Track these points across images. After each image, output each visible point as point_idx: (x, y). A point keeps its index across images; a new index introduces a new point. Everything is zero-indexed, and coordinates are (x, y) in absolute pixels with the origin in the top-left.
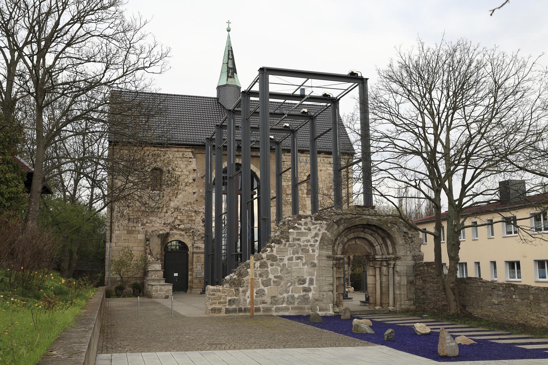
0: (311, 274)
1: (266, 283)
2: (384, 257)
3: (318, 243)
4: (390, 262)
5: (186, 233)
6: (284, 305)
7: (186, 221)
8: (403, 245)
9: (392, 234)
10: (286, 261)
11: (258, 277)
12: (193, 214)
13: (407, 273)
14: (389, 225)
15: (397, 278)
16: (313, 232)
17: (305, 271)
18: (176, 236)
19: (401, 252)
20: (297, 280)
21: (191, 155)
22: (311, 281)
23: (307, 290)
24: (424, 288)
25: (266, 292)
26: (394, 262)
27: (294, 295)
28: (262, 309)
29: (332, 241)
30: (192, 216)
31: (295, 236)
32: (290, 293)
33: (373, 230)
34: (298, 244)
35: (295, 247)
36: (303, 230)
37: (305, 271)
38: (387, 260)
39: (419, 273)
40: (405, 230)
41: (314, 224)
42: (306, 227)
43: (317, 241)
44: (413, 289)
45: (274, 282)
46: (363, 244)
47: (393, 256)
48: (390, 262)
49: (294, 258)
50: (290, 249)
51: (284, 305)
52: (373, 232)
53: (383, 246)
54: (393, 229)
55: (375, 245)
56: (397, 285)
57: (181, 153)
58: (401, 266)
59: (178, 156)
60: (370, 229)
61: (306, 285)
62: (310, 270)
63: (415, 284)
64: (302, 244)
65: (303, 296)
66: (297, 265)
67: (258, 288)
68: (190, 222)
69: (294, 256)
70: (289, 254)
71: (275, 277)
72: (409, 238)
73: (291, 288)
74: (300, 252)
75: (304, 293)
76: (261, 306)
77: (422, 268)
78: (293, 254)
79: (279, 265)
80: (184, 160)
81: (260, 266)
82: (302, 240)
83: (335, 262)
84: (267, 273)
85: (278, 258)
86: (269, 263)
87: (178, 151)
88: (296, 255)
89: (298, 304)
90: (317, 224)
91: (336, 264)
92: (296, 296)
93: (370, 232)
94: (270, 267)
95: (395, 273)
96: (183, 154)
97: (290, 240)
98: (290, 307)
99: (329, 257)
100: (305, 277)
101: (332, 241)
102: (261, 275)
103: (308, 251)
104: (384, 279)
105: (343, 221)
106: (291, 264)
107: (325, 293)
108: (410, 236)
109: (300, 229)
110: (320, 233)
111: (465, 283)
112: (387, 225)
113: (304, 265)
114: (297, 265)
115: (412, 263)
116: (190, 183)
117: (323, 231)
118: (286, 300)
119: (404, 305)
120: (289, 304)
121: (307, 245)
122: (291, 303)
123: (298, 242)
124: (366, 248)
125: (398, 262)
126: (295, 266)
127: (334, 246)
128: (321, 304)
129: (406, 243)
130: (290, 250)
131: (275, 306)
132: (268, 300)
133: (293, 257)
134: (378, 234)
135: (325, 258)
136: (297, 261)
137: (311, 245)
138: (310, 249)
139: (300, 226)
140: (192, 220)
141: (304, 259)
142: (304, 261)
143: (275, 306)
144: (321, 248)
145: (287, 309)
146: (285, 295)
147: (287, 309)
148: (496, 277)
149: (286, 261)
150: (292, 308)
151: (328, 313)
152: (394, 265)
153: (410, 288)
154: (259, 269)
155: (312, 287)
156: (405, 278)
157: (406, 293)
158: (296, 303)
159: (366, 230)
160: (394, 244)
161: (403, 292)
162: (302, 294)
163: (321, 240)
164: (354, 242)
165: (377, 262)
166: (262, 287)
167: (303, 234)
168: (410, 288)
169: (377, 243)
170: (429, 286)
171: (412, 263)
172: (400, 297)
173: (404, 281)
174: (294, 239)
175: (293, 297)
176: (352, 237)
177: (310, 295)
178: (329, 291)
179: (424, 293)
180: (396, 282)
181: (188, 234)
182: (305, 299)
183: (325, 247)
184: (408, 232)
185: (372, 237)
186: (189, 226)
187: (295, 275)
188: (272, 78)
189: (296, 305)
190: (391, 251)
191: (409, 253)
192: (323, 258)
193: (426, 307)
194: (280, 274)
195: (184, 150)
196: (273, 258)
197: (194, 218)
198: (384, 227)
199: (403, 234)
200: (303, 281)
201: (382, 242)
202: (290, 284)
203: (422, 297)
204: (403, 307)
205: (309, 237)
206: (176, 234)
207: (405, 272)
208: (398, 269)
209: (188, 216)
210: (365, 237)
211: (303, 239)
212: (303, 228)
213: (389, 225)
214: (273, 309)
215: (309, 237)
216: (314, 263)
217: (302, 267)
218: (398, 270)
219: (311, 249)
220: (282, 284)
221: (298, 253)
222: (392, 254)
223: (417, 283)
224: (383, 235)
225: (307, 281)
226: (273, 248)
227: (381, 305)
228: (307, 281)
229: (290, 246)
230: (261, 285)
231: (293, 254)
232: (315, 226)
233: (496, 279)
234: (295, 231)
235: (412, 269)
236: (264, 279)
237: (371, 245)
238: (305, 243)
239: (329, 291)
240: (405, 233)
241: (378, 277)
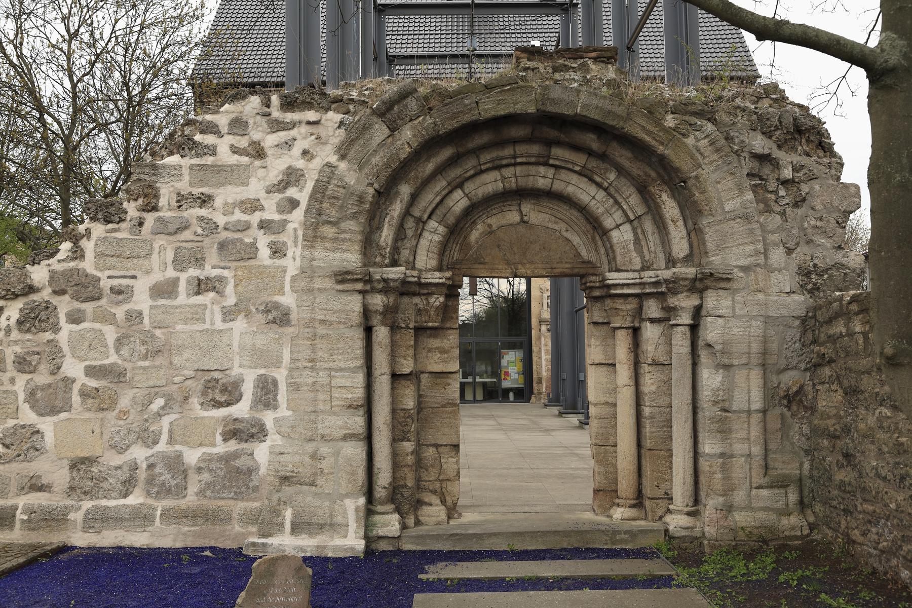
0: (260, 357)
1: (50, 401)
2: (649, 276)
3: (298, 215)
4: (673, 301)
6: (135, 499)
8: (747, 218)
9: (678, 160)
10: (142, 301)
11: (11, 371)
13: (764, 353)
14: (670, 121)
15: (710, 379)
16: (276, 166)
17: (238, 345)
19: (730, 251)
20: (196, 386)
22: (267, 393)
23: (245, 432)
24: (847, 430)
25: (49, 438)
26: (694, 301)
27: (179, 456)
28: (20, 516)
29: (361, 199)
31: (184, 185)
32: (162, 446)
33: (590, 153)
34: (201, 219)
35: (187, 235)
36: (225, 156)
37: (238, 345)
38: (663, 292)
39: (827, 350)
40: (760, 144)
41: (277, 126)
42: (243, 142)
43: (294, 204)
44: (799, 430)
45: (85, 394)
46: (562, 226)
47: (690, 271)
48: (673, 301)
49: (182, 287)
50: (160, 241)
51: (135, 499)
52: (593, 163)
53: (648, 225)
54: (690, 141)
55: (608, 223)
56: (708, 411)
58: (731, 320)
60: (576, 148)
61: (242, 409)
62: (261, 341)
63: (812, 409)
64: (221, 220)
65: (227, 459)
66: (197, 315)
67: (11, 423)
69: (183, 277)
70: (160, 265)
71: (91, 371)
72: (785, 183)
73: (166, 421)
74: (212, 256)
75: (233, 446)
76: (22, 501)
77: (839, 328)
78: (179, 263)
79: (108, 318)
81: (20, 323)
82: (218, 202)
84: (55, 353)
85: (106, 284)
86: (64, 305)
88: (193, 272)
89: (201, 493)
90: (293, 125)
92: (192, 457)
93: (580, 159)
94: (66, 329)
95: (703, 354)
97: (163, 202)
98: (160, 505)
99: (342, 277)
100: (236, 371)
101: (361, 199)
102: (23, 364)
103: (251, 251)
105: (412, 104)
106: (166, 310)
107: (324, 449)
108: (787, 173)
109: (212, 150)
110: (312, 170)
112: (658, 123)
113: (229, 315)
114: (197, 315)
115: (799, 302)
117: (327, 155)
118: (142, 475)
119: (749, 508)
120: (158, 496)
121: (247, 227)
122: (165, 491)
123: (203, 212)
124: (576, 240)
125: (712, 300)
126: (186, 321)
128: (307, 499)
129: (768, 210)
130: (164, 250)
131: (87, 504)
132: (60, 476)
133: (175, 282)
134: (621, 171)
135: (329, 283)
136: (199, 299)
137: (264, 225)
138: (263, 242)
139: (209, 139)
141: (230, 289)
142: (231, 300)
143: (87, 504)
144: (312, 237)
145: (141, 517)
146: (139, 454)
147: (141, 517)
149: (142, 301)
150: (167, 516)
151: (338, 542)
152: (697, 312)
153: (785, 428)
154: (15, 335)
155: (268, 418)
156: (756, 377)
157: (757, 450)
158: (193, 488)
159: (558, 152)
160: (692, 211)
161: (739, 448)
162: (221, 448)
163: (312, 197)
164: (513, 216)
165: (619, 304)
166: (28, 416)
167: (224, 174)
168: (785, 428)
169: (618, 216)
170: (872, 420)
171: (799, 302)
172: (725, 468)
173: (749, 391)
174: (182, 200)
175: (175, 464)
176: (490, 189)
177: (262, 453)
178: (346, 438)
179: (847, 456)
180: (705, 394)
182: (235, 476)
183: (329, 231)
184: (777, 154)
185: (593, 190)
187: (186, 362)
189: (191, 499)
190: (680, 246)
191: (777, 256)
192: (318, 283)
193: (856, 535)
194: (113, 358)
196: (83, 288)
198: (638, 128)
199: (748, 165)
200: (225, 390)
201: (640, 210)
202: (160, 402)
203: (840, 476)
204: (741, 518)
205: (255, 189)
207: (756, 347)
208: (712, 331)
210: (558, 186)
211: (224, 195)
212: (223, 145)
213: (670, 121)
214: (77, 517)
215: (255, 189)
216: (277, 306)
217: (219, 325)
219: (263, 242)
220: (124, 402)
221: (199, 261)
222: (688, 259)
223: (822, 403)
224: (636, 169)
225: (248, 390)
226: (84, 243)
227: (639, 500)
228: (248, 390)
229: (163, 229)
230: (25, 408)
231: (179, 263)
232: (283, 135)
234: (187, 162)
235: (794, 333)
236: (42, 378)
237: (596, 228)
238: (238, 216)
239: (346, 438)
240: (763, 158)
241: (624, 374)
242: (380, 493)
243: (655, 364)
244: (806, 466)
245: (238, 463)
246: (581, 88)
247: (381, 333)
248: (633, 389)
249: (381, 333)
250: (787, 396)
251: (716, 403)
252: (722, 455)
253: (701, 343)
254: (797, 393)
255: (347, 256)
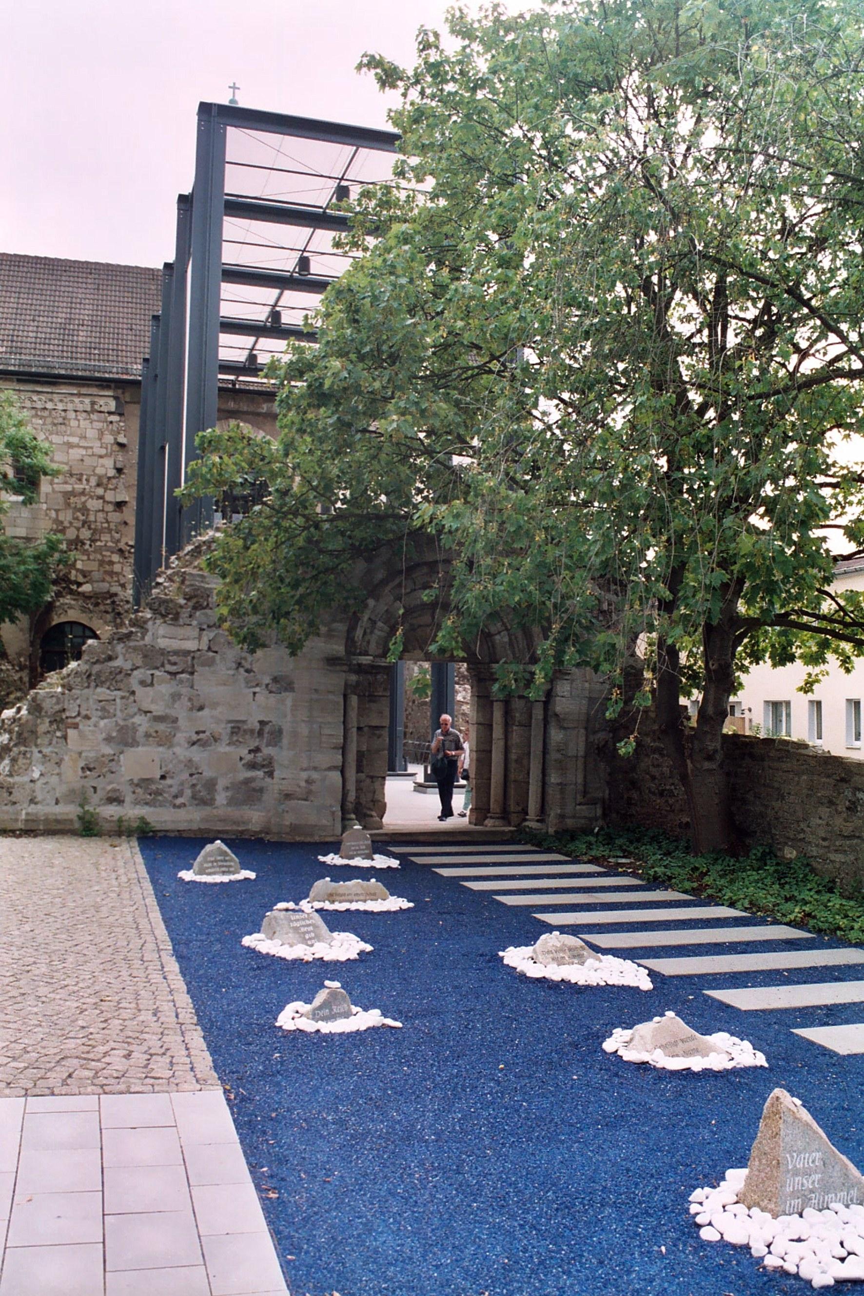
5: (97, 604)
7: (96, 575)
12: (116, 558)
15: (556, 735)
18: (71, 612)
21: (112, 405)
30: (111, 563)
56: (553, 756)
57: (87, 401)
59: (80, 407)
65: (247, 781)
68: (108, 578)
80: (94, 417)
83: (353, 678)
87: (79, 395)
89: (232, 802)
91: (358, 683)
96: (93, 403)
99: (332, 661)
104: (516, 733)
107: (315, 775)
111: (752, 756)
116: (109, 478)
119: (574, 817)
127: (352, 629)
140: (111, 573)
148: (820, 737)
172: (562, 792)
178: (330, 769)
181: (102, 607)
186: (104, 587)
188: (239, 141)
195: (94, 391)
197: (117, 568)
206: (71, 607)
209: (102, 563)
218: (558, 709)
233: (819, 742)
242: (350, 806)
243: (520, 725)
244: (607, 792)
245: (253, 785)
246: (81, 579)
247: (354, 700)
248: (509, 743)
249: (354, 700)
250: (598, 748)
251: (558, 751)
252: (561, 784)
253: (550, 713)
254: (604, 746)
255: (335, 647)
